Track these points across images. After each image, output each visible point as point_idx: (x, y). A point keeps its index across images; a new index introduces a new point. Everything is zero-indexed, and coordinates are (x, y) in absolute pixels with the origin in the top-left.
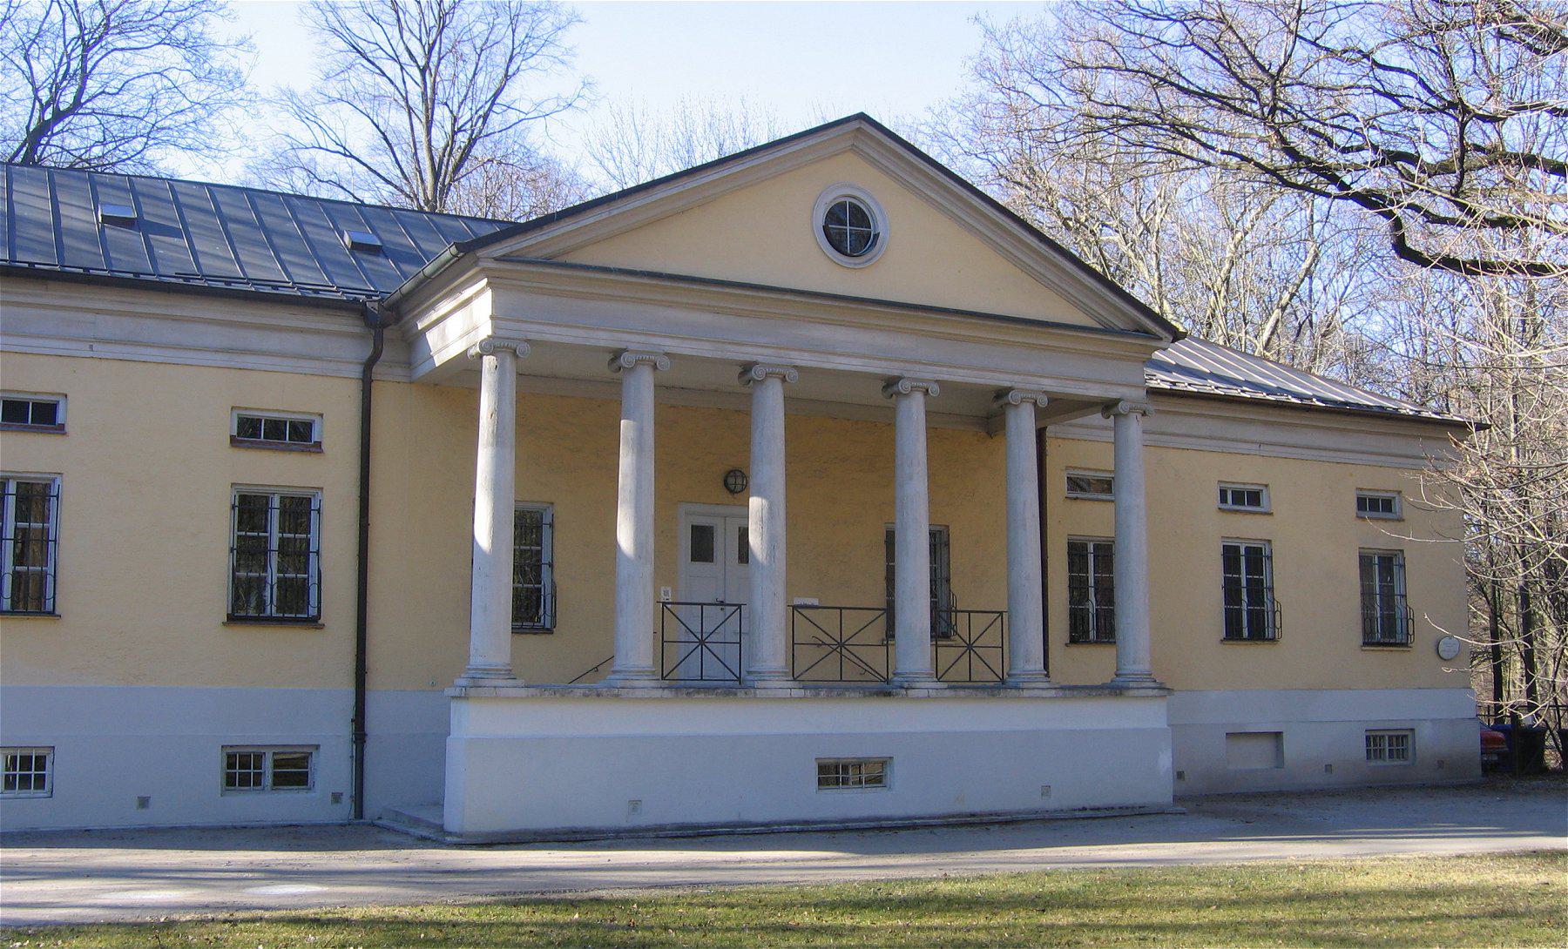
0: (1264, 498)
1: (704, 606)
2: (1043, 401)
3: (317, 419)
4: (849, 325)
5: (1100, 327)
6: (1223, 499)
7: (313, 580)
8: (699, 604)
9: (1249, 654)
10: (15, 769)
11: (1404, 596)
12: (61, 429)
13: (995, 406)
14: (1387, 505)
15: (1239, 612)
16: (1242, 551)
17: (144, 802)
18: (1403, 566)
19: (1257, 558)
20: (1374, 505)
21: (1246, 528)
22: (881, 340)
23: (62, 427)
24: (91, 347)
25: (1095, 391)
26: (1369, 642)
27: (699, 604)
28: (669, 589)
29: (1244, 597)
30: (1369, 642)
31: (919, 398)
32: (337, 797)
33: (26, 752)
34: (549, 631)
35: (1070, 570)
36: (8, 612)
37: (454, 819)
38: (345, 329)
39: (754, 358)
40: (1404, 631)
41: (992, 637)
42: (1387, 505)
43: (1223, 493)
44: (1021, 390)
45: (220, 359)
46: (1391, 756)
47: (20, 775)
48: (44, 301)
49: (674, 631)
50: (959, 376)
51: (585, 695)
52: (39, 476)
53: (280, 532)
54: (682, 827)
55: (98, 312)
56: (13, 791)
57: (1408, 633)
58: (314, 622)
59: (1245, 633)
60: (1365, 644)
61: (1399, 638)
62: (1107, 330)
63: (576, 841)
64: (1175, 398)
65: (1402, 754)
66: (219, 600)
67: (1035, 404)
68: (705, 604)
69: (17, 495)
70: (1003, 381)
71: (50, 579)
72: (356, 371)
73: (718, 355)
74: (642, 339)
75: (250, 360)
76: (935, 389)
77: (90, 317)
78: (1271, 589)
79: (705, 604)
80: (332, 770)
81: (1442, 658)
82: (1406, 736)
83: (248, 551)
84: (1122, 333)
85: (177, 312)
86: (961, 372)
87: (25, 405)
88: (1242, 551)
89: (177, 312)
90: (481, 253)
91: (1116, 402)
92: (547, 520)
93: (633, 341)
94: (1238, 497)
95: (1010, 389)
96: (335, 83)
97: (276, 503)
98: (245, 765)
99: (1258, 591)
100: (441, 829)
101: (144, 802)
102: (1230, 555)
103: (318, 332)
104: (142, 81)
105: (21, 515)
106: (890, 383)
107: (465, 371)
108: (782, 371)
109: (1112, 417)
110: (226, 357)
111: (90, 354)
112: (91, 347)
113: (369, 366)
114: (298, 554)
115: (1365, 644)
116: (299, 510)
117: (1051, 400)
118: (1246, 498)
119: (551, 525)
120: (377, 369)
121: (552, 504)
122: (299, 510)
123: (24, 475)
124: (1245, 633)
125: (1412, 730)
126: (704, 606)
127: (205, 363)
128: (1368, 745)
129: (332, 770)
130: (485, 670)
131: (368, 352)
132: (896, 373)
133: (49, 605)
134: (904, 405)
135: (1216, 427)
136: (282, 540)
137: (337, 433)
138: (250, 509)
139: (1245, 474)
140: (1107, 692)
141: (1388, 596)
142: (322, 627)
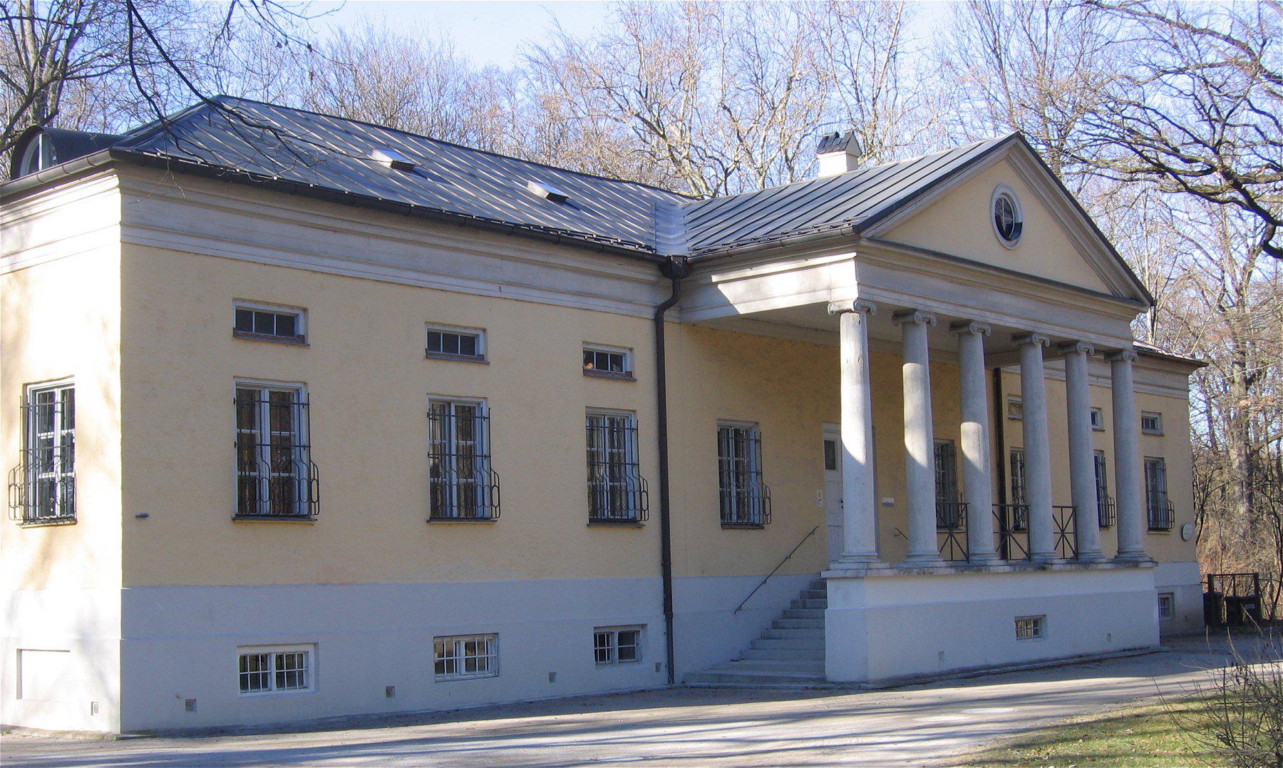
1: (1063, 509)
3: (628, 353)
4: (1012, 293)
5: (1111, 294)
8: (1059, 507)
9: (460, 535)
10: (258, 670)
12: (482, 359)
13: (1014, 344)
17: (552, 677)
23: (630, 374)
24: (500, 288)
26: (726, 524)
27: (1059, 507)
28: (820, 491)
32: (658, 666)
34: (759, 526)
36: (266, 515)
37: (834, 671)
38: (642, 277)
39: (972, 317)
40: (638, 507)
44: (978, 322)
45: (573, 301)
46: (280, 683)
47: (251, 674)
48: (473, 247)
51: (918, 574)
52: (254, 381)
53: (238, 428)
54: (962, 671)
55: (503, 258)
56: (483, 672)
57: (641, 509)
58: (634, 522)
59: (266, 507)
60: (1150, 529)
61: (1162, 525)
62: (1115, 297)
63: (924, 683)
67: (984, 333)
68: (1064, 507)
69: (270, 402)
72: (649, 313)
75: (592, 303)
76: (934, 320)
77: (497, 262)
79: (1064, 507)
80: (652, 645)
81: (1183, 539)
82: (1167, 598)
84: (1123, 300)
85: (552, 260)
86: (1058, 328)
89: (552, 260)
95: (1077, 341)
96: (866, 131)
97: (266, 396)
98: (255, 679)
100: (823, 680)
101: (190, 705)
103: (619, 278)
104: (1214, 257)
108: (984, 327)
109: (900, 325)
110: (575, 298)
111: (498, 294)
112: (500, 288)
115: (1150, 529)
117: (993, 332)
121: (757, 423)
123: (464, 399)
124: (266, 507)
125: (1172, 593)
126: (1063, 509)
127: (250, 258)
128: (243, 668)
129: (652, 645)
130: (868, 556)
137: (642, 363)
140: (1131, 565)
141: (469, 457)
142: (641, 527)
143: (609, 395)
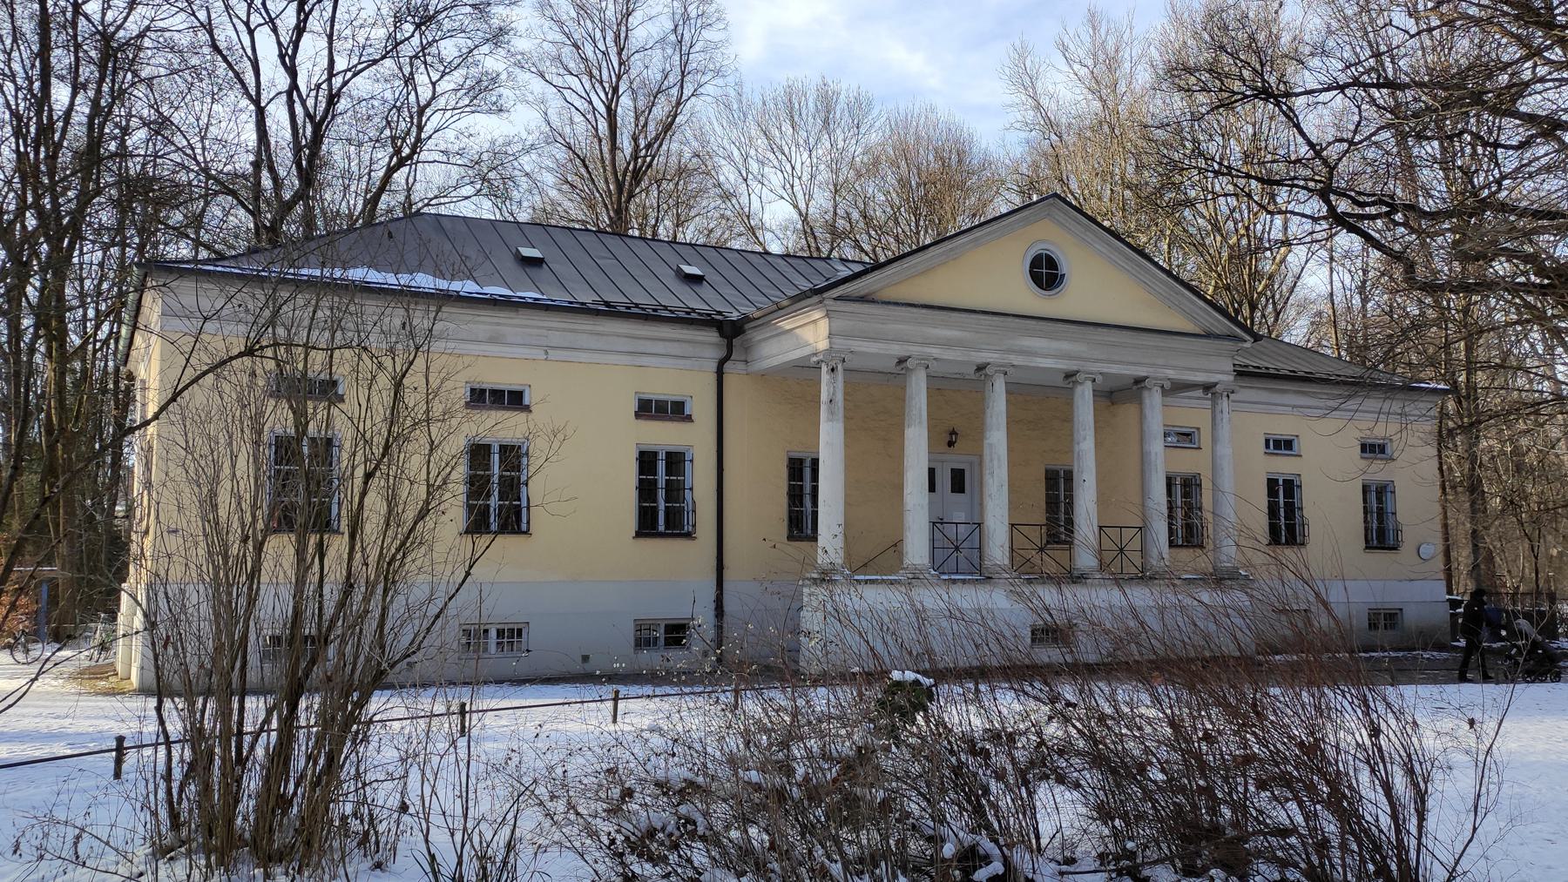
0: (1295, 445)
2: (1167, 385)
6: (1267, 446)
7: (524, 503)
11: (1394, 514)
12: (689, 418)
14: (1382, 449)
15: (655, 510)
16: (1281, 482)
18: (1393, 492)
19: (1291, 487)
20: (1371, 449)
21: (1283, 466)
22: (1065, 346)
25: (1201, 378)
26: (1368, 547)
29: (1282, 513)
30: (1368, 547)
31: (1089, 384)
33: (511, 626)
35: (641, 473)
41: (1136, 544)
42: (1382, 449)
43: (1267, 441)
46: (1386, 628)
49: (1107, 544)
50: (1114, 369)
55: (550, 329)
60: (1367, 548)
62: (1208, 335)
64: (1372, 404)
65: (1393, 626)
66: (631, 521)
70: (1141, 372)
71: (524, 511)
72: (713, 366)
73: (966, 359)
74: (920, 349)
75: (645, 360)
78: (1301, 509)
83: (646, 490)
87: (483, 391)
88: (1281, 482)
90: (826, 295)
91: (1215, 384)
92: (524, 450)
93: (913, 350)
94: (1277, 444)
99: (1291, 509)
101: (585, 658)
102: (1272, 484)
105: (669, 472)
106: (1069, 375)
107: (805, 371)
113: (721, 364)
114: (676, 491)
116: (676, 461)
118: (1282, 445)
119: (691, 461)
120: (728, 366)
122: (676, 461)
131: (722, 353)
132: (1075, 368)
133: (524, 527)
134: (1079, 389)
135: (1263, 396)
136: (501, 477)
137: (702, 407)
138: (646, 461)
139: (1379, 432)
143: (663, 435)
